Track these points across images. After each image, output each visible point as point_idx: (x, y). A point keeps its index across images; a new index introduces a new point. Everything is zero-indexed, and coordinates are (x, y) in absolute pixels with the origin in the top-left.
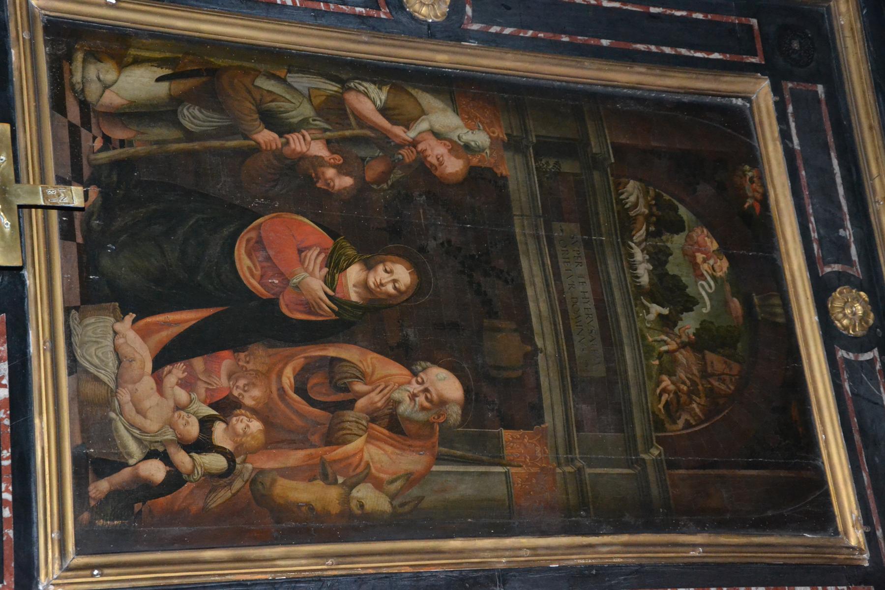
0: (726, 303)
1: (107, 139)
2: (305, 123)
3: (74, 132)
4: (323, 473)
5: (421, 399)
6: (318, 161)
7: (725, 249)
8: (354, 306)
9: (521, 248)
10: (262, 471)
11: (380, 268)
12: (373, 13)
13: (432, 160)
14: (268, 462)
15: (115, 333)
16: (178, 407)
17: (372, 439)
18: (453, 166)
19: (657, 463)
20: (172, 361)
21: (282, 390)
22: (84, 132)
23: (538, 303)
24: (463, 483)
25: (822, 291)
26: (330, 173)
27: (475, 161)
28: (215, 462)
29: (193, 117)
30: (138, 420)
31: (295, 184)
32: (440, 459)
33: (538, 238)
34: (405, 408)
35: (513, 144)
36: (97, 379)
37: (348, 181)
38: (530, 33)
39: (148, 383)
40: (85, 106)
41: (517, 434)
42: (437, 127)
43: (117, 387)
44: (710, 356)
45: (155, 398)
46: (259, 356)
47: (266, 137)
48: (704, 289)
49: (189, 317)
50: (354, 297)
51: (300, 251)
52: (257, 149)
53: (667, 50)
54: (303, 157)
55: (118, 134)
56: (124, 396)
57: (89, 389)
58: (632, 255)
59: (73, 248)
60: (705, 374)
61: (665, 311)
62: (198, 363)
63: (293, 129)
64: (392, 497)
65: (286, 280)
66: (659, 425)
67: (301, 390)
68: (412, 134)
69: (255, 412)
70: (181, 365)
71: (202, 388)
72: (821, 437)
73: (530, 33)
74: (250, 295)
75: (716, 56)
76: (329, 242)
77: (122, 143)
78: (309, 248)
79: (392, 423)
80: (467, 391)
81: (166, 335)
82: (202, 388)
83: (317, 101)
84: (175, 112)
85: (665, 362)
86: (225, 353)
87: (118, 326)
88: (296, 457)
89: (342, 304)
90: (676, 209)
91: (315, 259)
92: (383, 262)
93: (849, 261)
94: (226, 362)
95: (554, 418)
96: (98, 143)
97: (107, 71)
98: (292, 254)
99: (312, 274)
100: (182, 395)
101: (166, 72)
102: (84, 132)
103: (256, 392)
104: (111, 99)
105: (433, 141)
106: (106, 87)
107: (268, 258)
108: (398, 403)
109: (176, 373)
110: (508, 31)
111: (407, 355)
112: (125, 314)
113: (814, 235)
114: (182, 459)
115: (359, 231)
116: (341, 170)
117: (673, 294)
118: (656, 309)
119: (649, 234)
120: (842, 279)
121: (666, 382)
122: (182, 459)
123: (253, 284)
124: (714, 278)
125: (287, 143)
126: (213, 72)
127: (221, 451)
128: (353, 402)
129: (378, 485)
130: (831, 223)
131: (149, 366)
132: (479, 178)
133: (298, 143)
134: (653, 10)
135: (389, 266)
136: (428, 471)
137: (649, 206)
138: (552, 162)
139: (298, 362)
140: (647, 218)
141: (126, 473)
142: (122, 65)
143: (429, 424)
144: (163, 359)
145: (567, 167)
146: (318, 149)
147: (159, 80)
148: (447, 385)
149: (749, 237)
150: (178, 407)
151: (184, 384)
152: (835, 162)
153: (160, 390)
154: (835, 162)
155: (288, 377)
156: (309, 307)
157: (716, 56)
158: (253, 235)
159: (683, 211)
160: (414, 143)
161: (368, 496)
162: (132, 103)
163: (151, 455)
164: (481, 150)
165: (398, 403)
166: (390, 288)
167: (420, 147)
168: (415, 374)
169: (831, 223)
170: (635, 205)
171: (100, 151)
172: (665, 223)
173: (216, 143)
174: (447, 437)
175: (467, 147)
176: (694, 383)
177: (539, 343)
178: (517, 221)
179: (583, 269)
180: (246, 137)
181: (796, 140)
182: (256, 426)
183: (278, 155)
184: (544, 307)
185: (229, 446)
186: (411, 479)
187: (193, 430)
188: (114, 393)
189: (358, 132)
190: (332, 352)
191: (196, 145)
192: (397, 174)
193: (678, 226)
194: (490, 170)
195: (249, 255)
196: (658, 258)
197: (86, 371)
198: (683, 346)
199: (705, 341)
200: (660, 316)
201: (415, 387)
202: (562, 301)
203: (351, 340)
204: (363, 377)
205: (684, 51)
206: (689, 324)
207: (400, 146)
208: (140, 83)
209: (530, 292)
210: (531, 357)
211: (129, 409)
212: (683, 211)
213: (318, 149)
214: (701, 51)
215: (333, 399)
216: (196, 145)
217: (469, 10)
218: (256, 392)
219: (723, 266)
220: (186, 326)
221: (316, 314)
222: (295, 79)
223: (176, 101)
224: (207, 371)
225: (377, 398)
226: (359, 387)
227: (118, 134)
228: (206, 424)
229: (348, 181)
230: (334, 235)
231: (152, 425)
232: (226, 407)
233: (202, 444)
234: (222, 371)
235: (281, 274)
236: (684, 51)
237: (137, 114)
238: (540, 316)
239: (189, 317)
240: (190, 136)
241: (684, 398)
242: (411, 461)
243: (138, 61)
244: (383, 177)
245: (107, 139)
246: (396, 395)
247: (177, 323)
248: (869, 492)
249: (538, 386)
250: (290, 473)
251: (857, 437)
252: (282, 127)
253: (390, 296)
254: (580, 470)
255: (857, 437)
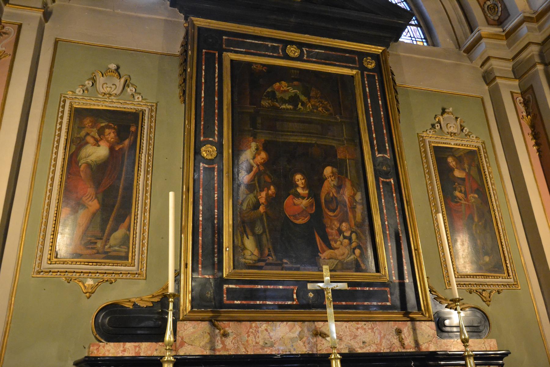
0: (295, 85)
1: (268, 255)
2: (256, 197)
3: (267, 264)
4: (353, 208)
5: (333, 178)
6: (267, 194)
7: (279, 81)
8: (309, 192)
9: (286, 140)
10: (355, 224)
11: (297, 183)
12: (216, 170)
13: (262, 161)
14: (353, 222)
15: (324, 259)
16: (341, 244)
17: (343, 194)
18: (263, 155)
19: (341, 118)
20: (330, 245)
21: (335, 216)
22: (267, 261)
23: (302, 140)
24: (351, 171)
25: (287, 57)
26: (270, 192)
27: (261, 148)
28: (354, 236)
29: (259, 230)
30: (346, 255)
31: (275, 203)
32: (347, 176)
33: (282, 135)
34: (335, 183)
35: (255, 137)
36: (337, 265)
37: (272, 187)
38: (216, 122)
39: (336, 251)
40: (259, 260)
41: (338, 154)
42: (252, 157)
43: (338, 259)
44: (311, 95)
45: (340, 250)
46: (327, 221)
47: (262, 209)
48: (292, 91)
49: (318, 239)
50: (307, 192)
51: (295, 205)
52: (266, 212)
53: (217, 80)
54: (266, 199)
55: (266, 252)
56: (340, 258)
57: (339, 267)
58: (284, 109)
59: (302, 267)
60: (316, 98)
61: (300, 104)
62: (330, 238)
63: (258, 201)
64: (357, 191)
65: (304, 210)
66: (331, 114)
67: (334, 211)
68: (255, 165)
69: (341, 224)
70: (331, 242)
71: (336, 237)
72: (330, 71)
73: (216, 122)
74: (309, 221)
75: (217, 65)
76: (291, 197)
77: (269, 251)
78: (294, 202)
79: (339, 187)
80: (329, 165)
81: (323, 246)
82: (336, 237)
83: (249, 193)
84: (258, 235)
85: (314, 106)
86: (326, 230)
87: (322, 258)
88: (350, 215)
89: (309, 195)
90: (268, 92)
91: (297, 201)
92: (295, 182)
93: (279, 53)
94: (329, 230)
95: (334, 143)
96: (270, 258)
97: (248, 253)
98: (296, 207)
99: (302, 203)
100: (338, 243)
101: (245, 235)
102: (267, 261)
103: (336, 223)
104: (256, 252)
105: (256, 160)
106: (252, 254)
107: (299, 214)
108: (334, 185)
109: (333, 243)
110: (216, 128)
111: (322, 180)
112: (319, 256)
113: (271, 54)
114: (354, 245)
115: (286, 188)
116: (269, 189)
117: (294, 100)
118: (300, 106)
119: (277, 102)
120: (284, 50)
121: (320, 109)
122: (354, 245)
123: (306, 220)
124: (288, 87)
125: (263, 203)
126: (243, 222)
127: (351, 234)
128: (335, 197)
129: (355, 194)
130: (267, 48)
131: (332, 251)
132: (266, 147)
133: (262, 200)
134: (203, 81)
135: (296, 180)
136: (350, 180)
137: (268, 99)
138: (258, 125)
139: (326, 210)
140: (272, 101)
141: (359, 259)
142: (244, 248)
143: (339, 177)
144: (330, 247)
145: (259, 121)
146: (264, 194)
147: (248, 238)
148: (328, 171)
149: (275, 74)
150: (341, 244)
151: (336, 242)
152: (248, 41)
153: (338, 248)
154: (248, 41)
155: (331, 214)
156: (311, 205)
157: (217, 65)
158: (292, 217)
159: (269, 90)
160: (258, 165)
161: (358, 197)
162: (257, 247)
163: (354, 253)
164: (257, 145)
165: (334, 185)
166: (303, 181)
167: (259, 164)
168: (326, 179)
169: (267, 48)
170: (269, 103)
171: (272, 257)
172: (272, 96)
173: (266, 224)
174: (340, 172)
175: (257, 149)
176: (319, 101)
177: (314, 142)
178: (278, 140)
179: (290, 124)
180: (263, 215)
181: (242, 50)
182: (344, 224)
183: (267, 207)
184: (303, 138)
185: (349, 232)
186: (353, 186)
187: (346, 241)
188: (340, 261)
189: (256, 182)
190: (323, 201)
191: (267, 230)
192: (268, 172)
193: (273, 93)
194: (263, 144)
195: (297, 220)
196: (284, 101)
197: (335, 267)
198: (310, 102)
199: (306, 93)
200: (302, 105)
201: (330, 179)
202: (301, 133)
203: (319, 195)
204: (328, 193)
205: (216, 75)
206: (303, 98)
207: (259, 170)
208: (250, 243)
209: (299, 141)
210: (318, 146)
211: (343, 257)
212: (269, 90)
213: (264, 194)
214: (215, 70)
215: (330, 201)
216: (267, 230)
217: (211, 139)
218: (336, 223)
219: (284, 83)
220: (321, 240)
221: (313, 204)
222: (241, 199)
223: (254, 234)
224: (332, 236)
225: (334, 191)
226: (331, 195)
227: (266, 252)
228: (345, 237)
229: (272, 187)
230: (289, 195)
231: (347, 252)
232: (340, 232)
233: (350, 239)
234: (332, 232)
235: (303, 211)
236: (216, 75)
237: (259, 245)
238: (307, 140)
239: (318, 239)
240: (264, 232)
241: (323, 106)
242: (348, 184)
243: (243, 244)
244: (270, 177)
245: (268, 255)
246: (332, 185)
247: (320, 244)
248: (341, 64)
249: (325, 145)
250: (355, 218)
251: (327, 62)
252: (257, 205)
253: (305, 181)
254: (345, 139)
255: (327, 62)
